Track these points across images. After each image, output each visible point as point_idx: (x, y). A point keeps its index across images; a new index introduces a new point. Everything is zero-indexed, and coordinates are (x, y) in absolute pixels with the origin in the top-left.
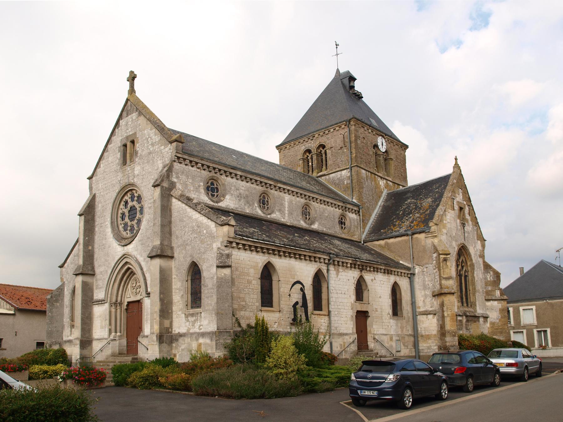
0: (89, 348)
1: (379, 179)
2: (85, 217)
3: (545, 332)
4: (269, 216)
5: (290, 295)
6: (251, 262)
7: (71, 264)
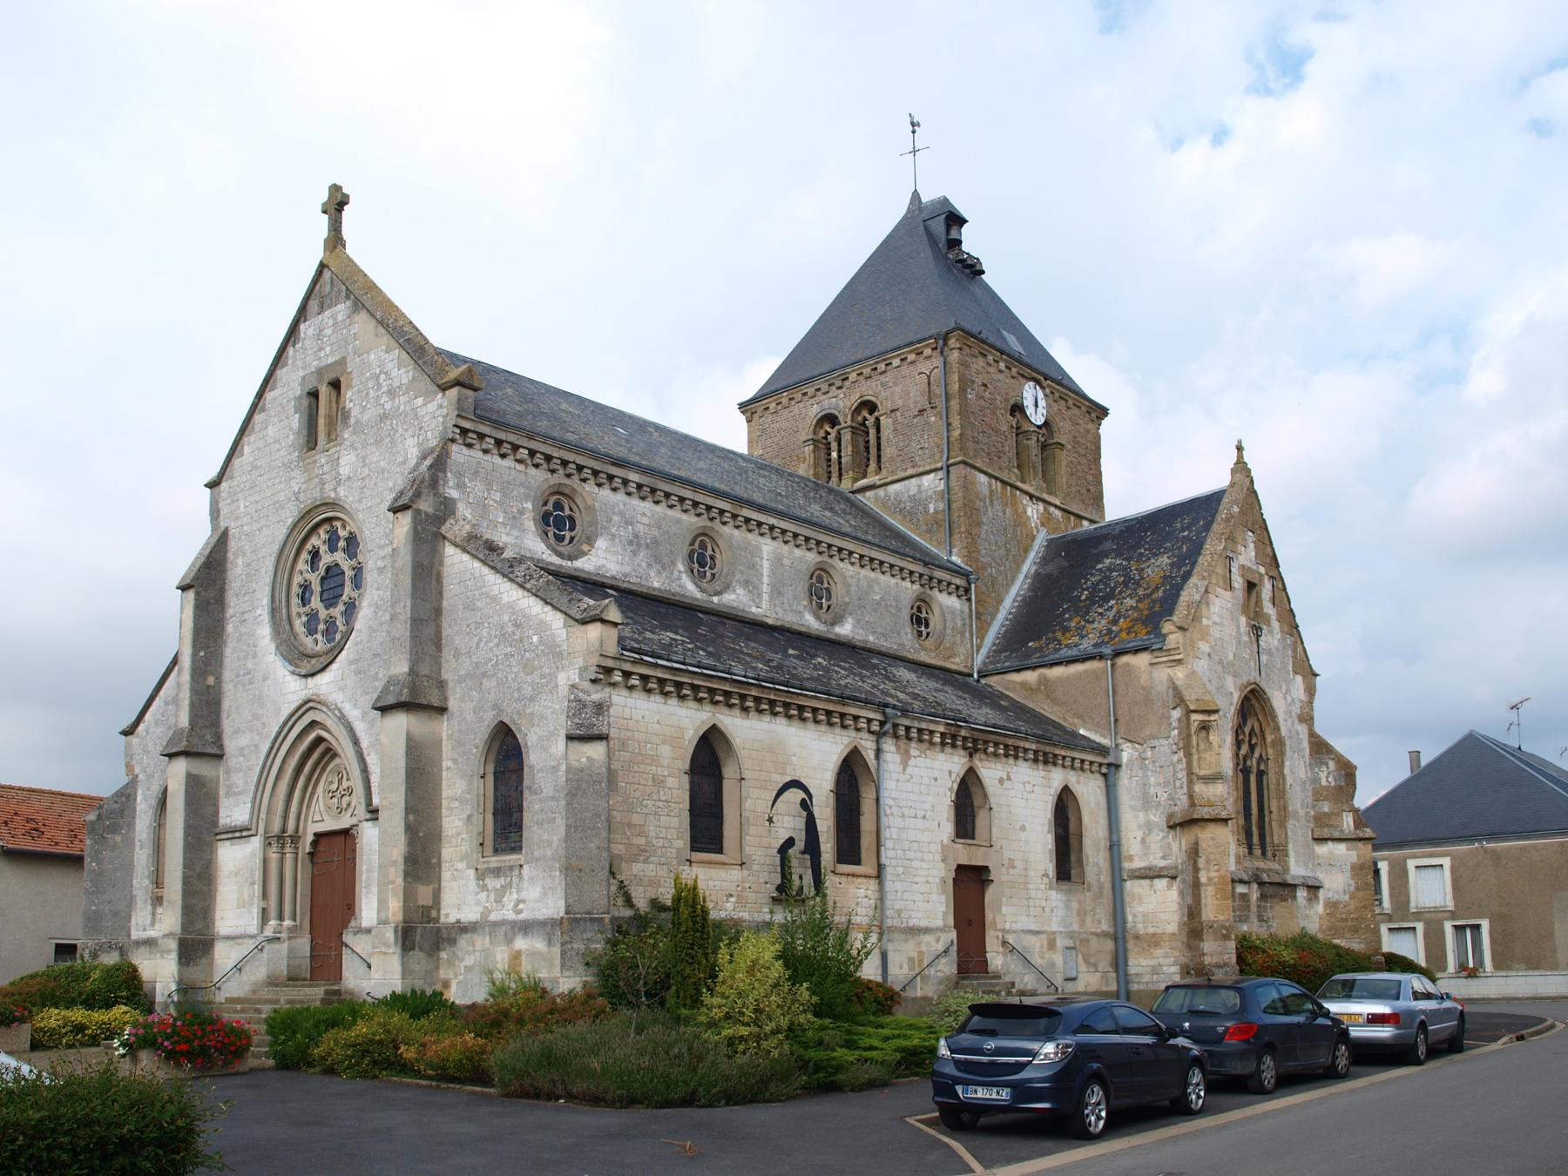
1: (1025, 500)
2: (197, 594)
4: (715, 599)
5: (770, 820)
6: (663, 725)
7: (157, 723)
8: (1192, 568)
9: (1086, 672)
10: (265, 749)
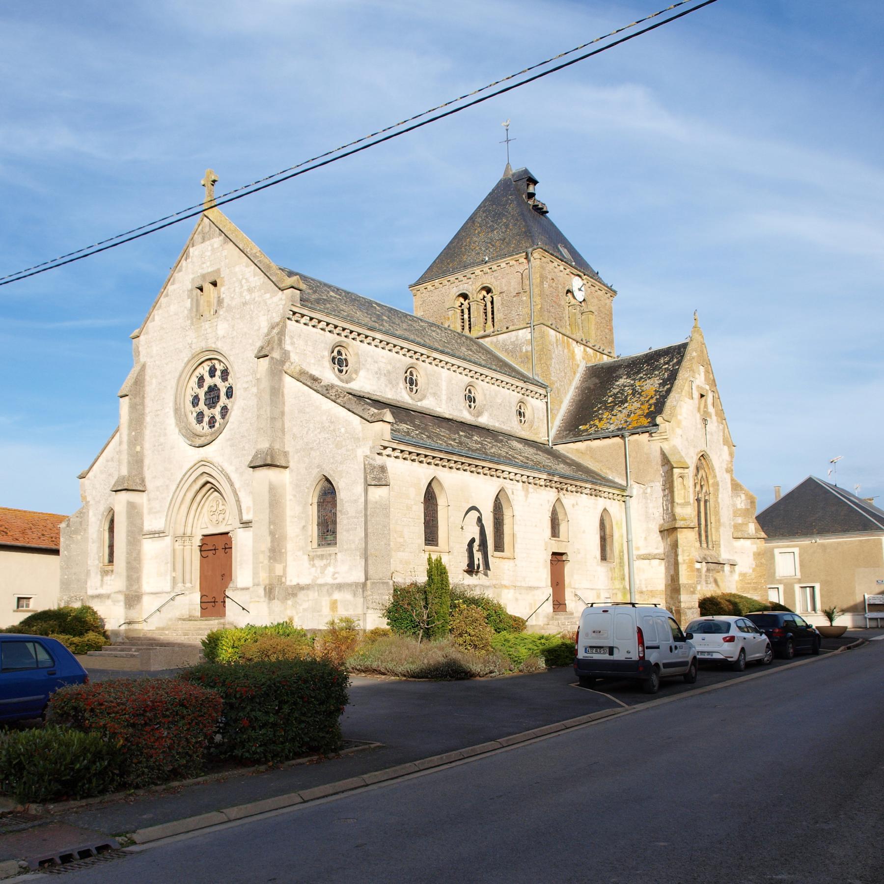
0: (138, 607)
3: (813, 587)
4: (419, 404)
5: (462, 528)
6: (409, 475)
8: (672, 387)
9: (613, 444)
10: (174, 487)
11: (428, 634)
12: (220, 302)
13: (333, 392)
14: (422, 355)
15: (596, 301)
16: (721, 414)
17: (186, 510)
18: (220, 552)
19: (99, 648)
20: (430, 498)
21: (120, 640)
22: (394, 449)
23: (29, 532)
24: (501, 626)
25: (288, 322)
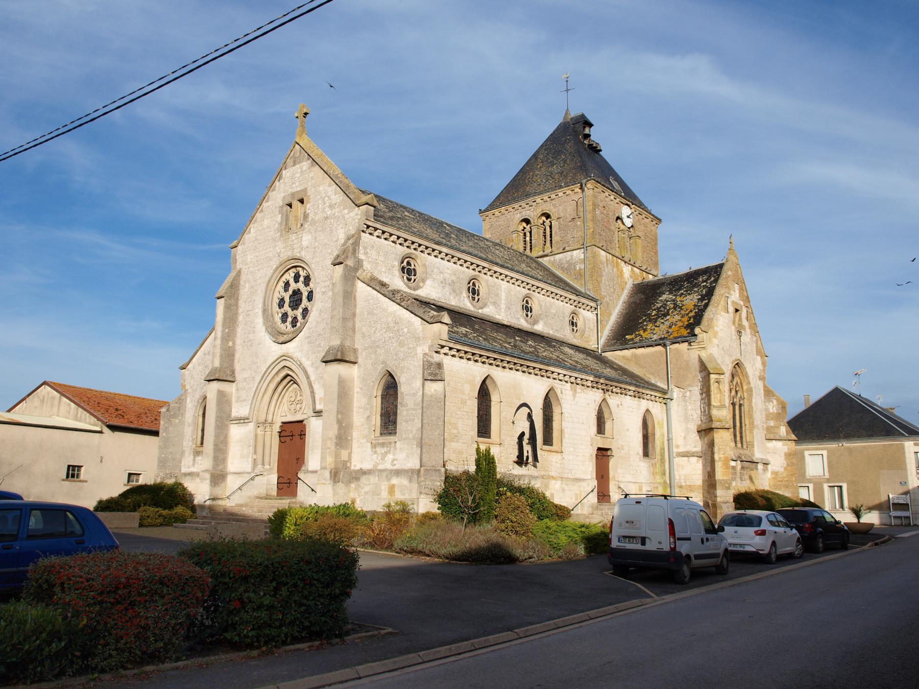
0: (223, 485)
3: (841, 487)
4: (480, 311)
5: (513, 423)
6: (464, 373)
7: (199, 365)
9: (656, 352)
11: (475, 519)
12: (306, 216)
13: (398, 296)
14: (484, 268)
15: (642, 227)
16: (754, 328)
17: (268, 400)
18: (297, 438)
19: (184, 521)
20: (484, 395)
21: (204, 514)
22: (451, 349)
23: (144, 416)
24: (544, 514)
25: (363, 234)
